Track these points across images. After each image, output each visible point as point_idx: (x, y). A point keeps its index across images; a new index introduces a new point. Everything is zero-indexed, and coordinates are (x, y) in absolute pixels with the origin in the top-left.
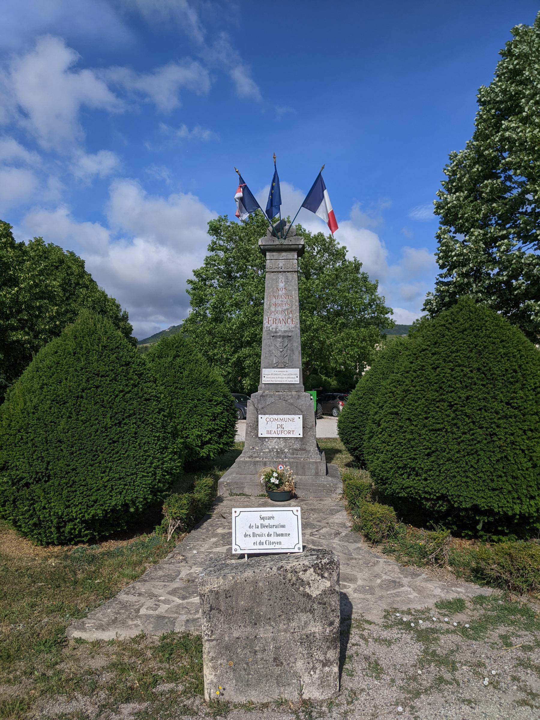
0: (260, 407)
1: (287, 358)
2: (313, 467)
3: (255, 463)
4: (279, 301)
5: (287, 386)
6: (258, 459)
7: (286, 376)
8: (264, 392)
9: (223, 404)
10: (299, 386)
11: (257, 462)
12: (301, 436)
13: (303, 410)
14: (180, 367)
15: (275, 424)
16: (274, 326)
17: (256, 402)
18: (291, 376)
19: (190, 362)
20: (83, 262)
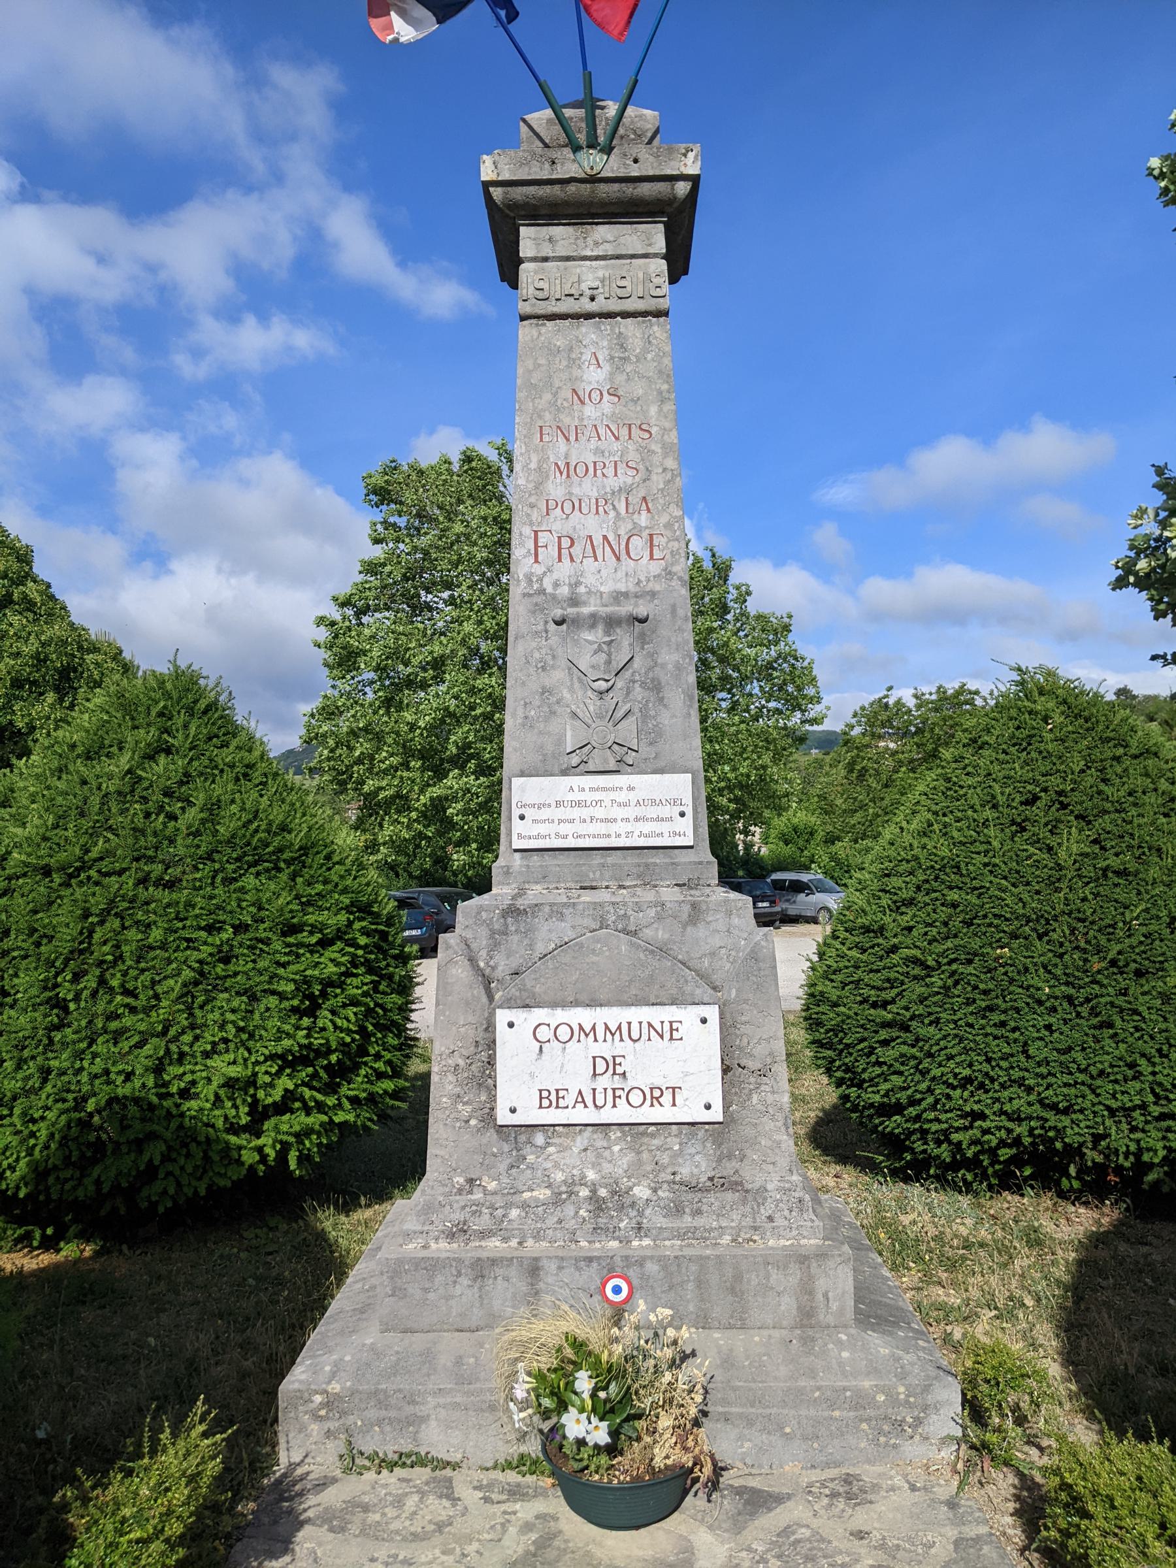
0: (503, 965)
1: (630, 724)
2: (787, 1280)
3: (482, 1269)
4: (584, 453)
5: (632, 859)
6: (494, 1244)
7: (630, 812)
8: (521, 892)
9: (353, 943)
10: (690, 856)
11: (493, 1262)
12: (716, 1114)
13: (717, 978)
14: (168, 793)
15: (580, 1054)
16: (564, 570)
17: (481, 942)
18: (652, 812)
19: (213, 771)
20: (29, 550)
